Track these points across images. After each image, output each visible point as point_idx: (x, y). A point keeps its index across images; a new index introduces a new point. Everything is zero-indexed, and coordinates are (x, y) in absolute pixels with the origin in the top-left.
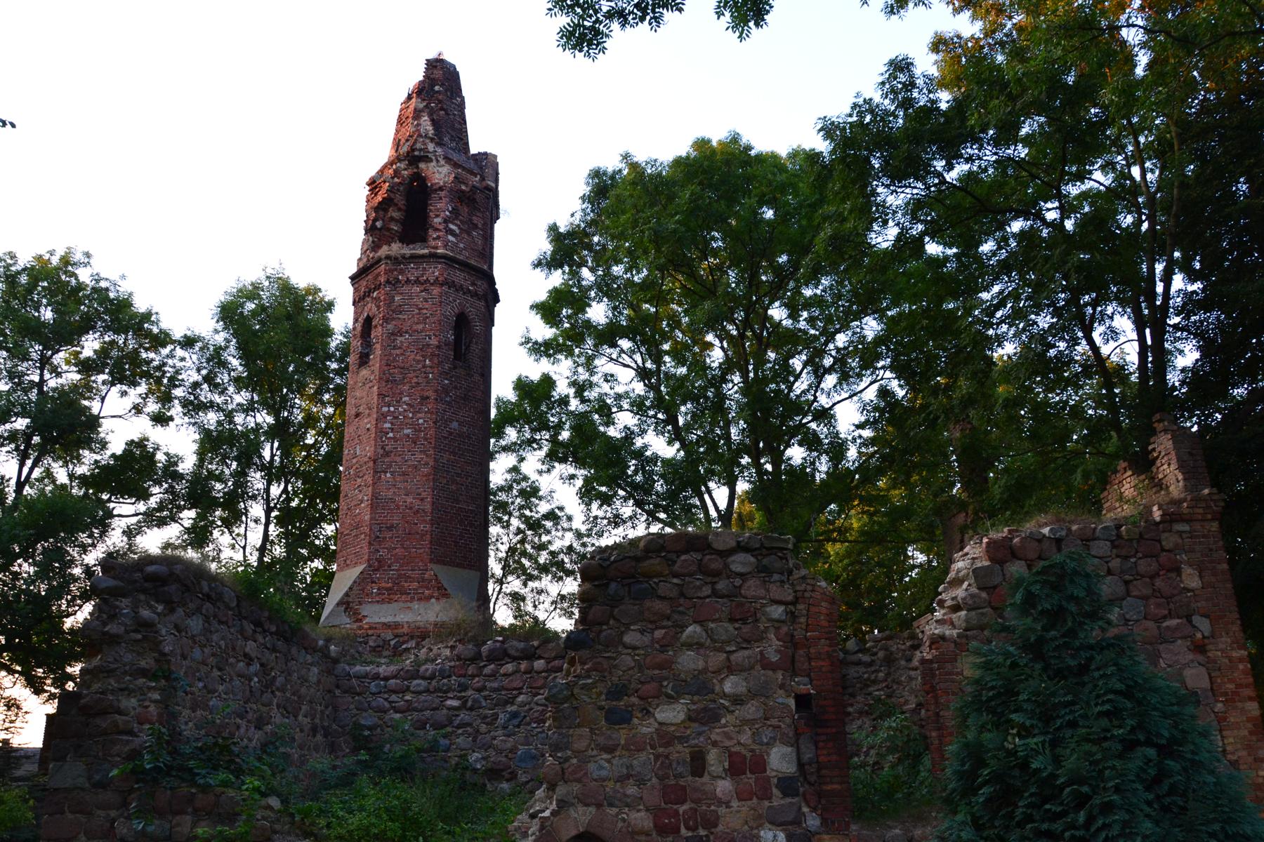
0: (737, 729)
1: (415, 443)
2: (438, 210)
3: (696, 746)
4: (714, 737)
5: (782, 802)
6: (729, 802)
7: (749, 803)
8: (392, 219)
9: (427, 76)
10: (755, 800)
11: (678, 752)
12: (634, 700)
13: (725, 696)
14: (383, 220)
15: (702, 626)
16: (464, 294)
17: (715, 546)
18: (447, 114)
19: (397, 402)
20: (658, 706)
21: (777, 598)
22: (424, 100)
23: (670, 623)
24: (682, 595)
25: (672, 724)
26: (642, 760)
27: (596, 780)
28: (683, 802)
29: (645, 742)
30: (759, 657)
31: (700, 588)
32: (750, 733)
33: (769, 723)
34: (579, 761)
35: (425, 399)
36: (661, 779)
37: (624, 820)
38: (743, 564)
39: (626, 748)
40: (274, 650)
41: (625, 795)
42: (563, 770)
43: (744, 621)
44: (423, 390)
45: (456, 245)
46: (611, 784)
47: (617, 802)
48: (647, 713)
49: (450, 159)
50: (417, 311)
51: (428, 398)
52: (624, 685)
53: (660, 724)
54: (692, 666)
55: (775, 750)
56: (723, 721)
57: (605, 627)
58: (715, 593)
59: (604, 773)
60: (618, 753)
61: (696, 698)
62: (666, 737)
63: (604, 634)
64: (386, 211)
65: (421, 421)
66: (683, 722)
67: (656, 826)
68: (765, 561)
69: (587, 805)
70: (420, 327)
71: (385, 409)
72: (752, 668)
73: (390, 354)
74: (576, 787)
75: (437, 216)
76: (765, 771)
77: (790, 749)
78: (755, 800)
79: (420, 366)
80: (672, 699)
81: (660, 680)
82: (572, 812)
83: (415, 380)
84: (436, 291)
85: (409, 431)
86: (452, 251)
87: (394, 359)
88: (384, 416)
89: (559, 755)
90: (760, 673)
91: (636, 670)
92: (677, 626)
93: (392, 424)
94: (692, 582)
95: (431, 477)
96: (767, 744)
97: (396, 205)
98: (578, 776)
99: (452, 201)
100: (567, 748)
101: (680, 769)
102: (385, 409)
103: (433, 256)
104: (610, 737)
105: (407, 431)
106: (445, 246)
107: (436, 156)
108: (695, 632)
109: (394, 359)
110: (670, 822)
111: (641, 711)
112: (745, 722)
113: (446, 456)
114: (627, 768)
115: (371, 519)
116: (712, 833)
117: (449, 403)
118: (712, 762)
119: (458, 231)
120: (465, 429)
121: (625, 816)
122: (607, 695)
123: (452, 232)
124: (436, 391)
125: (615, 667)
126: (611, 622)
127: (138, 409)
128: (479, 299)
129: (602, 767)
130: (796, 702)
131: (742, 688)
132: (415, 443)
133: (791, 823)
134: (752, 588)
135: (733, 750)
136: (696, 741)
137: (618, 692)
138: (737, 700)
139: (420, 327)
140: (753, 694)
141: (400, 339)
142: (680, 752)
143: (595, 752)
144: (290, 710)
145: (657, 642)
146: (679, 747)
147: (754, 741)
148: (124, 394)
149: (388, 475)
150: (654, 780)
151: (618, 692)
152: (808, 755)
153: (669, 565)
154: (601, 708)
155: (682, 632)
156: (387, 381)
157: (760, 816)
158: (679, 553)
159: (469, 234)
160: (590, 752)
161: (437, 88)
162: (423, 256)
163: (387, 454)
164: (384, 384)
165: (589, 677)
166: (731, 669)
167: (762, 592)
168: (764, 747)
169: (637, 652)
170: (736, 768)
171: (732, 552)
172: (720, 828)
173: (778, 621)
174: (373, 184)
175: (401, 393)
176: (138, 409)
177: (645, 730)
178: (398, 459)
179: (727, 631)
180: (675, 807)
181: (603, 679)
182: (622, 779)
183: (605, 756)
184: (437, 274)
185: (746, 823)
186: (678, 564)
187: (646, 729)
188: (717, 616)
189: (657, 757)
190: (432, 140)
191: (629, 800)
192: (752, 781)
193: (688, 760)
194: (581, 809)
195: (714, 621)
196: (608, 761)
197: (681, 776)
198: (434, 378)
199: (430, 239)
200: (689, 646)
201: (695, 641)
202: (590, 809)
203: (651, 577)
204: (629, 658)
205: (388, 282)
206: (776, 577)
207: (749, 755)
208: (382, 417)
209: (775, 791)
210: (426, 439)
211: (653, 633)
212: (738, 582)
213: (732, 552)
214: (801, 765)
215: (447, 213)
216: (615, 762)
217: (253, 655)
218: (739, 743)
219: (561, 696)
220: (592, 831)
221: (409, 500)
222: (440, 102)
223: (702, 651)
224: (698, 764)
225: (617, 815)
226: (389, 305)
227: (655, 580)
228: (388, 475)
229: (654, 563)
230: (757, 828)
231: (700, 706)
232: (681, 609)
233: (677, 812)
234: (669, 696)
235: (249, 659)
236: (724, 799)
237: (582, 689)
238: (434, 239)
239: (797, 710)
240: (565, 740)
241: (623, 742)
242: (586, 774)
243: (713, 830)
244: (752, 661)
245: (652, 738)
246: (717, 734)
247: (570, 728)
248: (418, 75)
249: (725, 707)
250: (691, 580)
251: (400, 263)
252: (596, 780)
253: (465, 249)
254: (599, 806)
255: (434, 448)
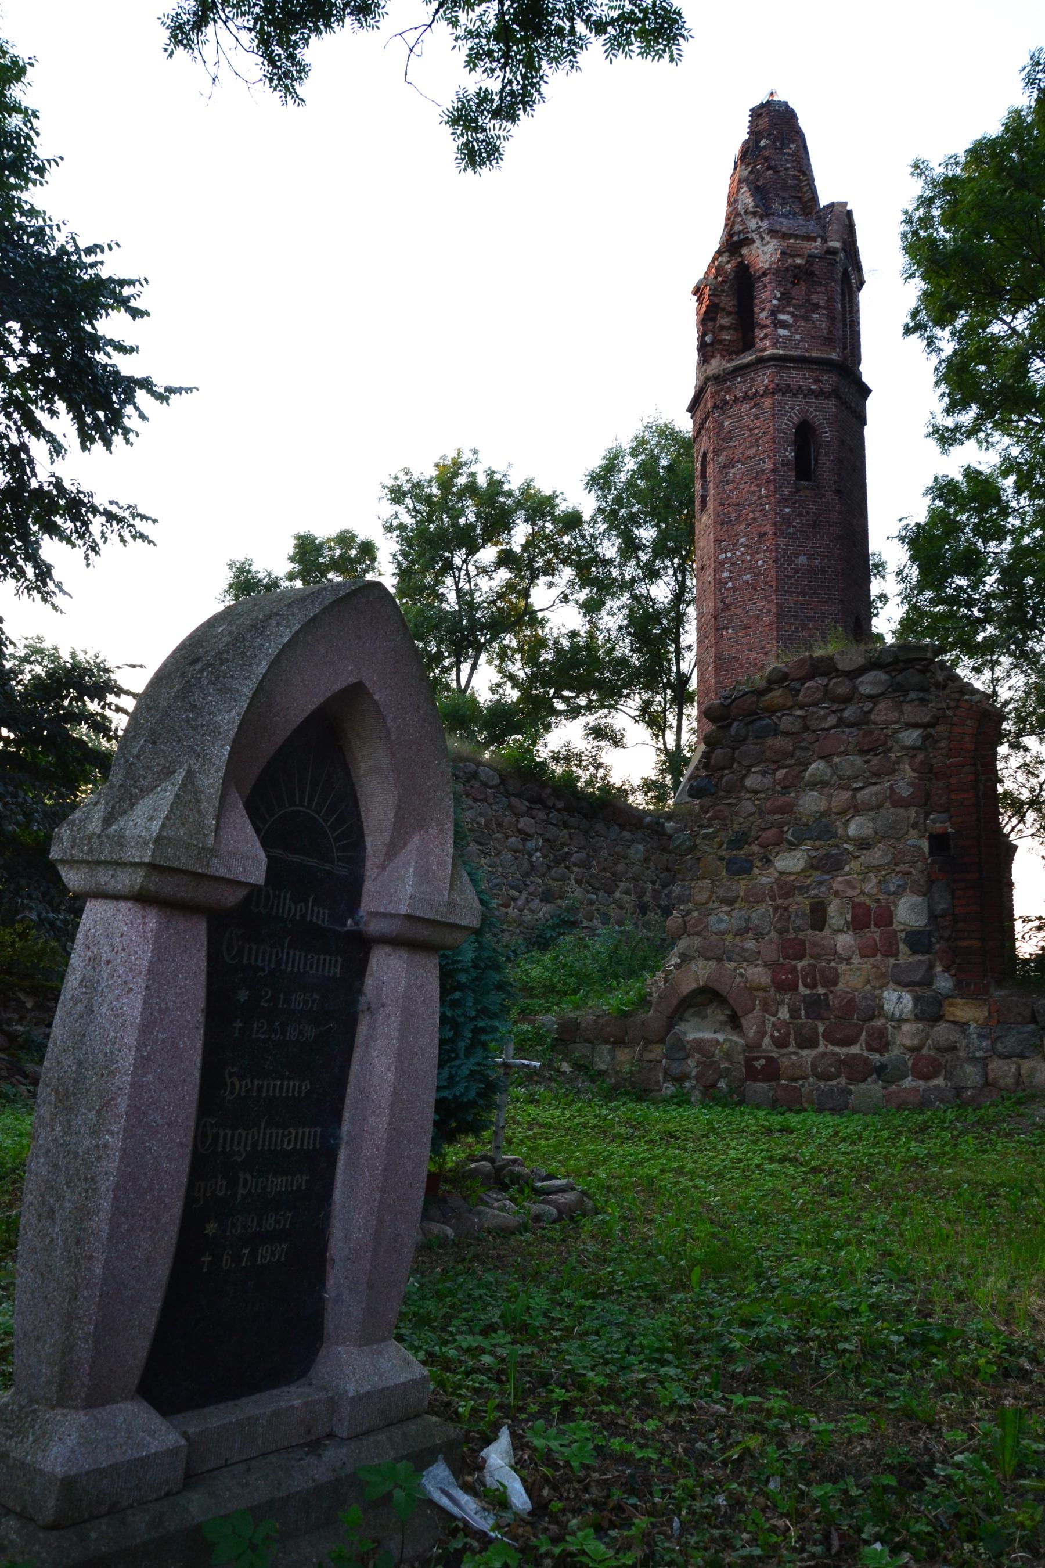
0: (860, 877)
1: (755, 589)
2: (763, 302)
3: (816, 896)
4: (836, 886)
5: (910, 960)
6: (850, 958)
7: (872, 959)
8: (722, 328)
9: (755, 133)
10: (879, 957)
11: (797, 904)
12: (755, 848)
13: (849, 840)
14: (713, 332)
15: (827, 761)
16: (805, 396)
17: (840, 666)
18: (776, 172)
19: (735, 545)
20: (777, 854)
21: (912, 720)
22: (749, 164)
23: (793, 761)
24: (806, 728)
25: (791, 874)
26: (761, 913)
27: (715, 933)
28: (801, 958)
29: (764, 893)
30: (888, 792)
31: (825, 718)
32: (875, 881)
33: (898, 869)
34: (700, 914)
35: (762, 535)
36: (780, 932)
37: (742, 975)
38: (874, 684)
39: (745, 900)
40: (566, 825)
41: (743, 950)
42: (685, 923)
43: (872, 750)
44: (760, 526)
45: (789, 338)
46: (729, 938)
47: (735, 957)
48: (768, 862)
49: (777, 232)
50: (748, 433)
51: (765, 534)
52: (744, 833)
53: (781, 873)
54: (815, 808)
55: (903, 900)
56: (847, 868)
57: (726, 772)
58: (841, 723)
59: (723, 926)
60: (737, 905)
61: (818, 843)
62: (786, 888)
63: (725, 779)
64: (714, 319)
65: (760, 563)
66: (803, 871)
67: (773, 981)
68: (900, 678)
69: (708, 959)
70: (753, 451)
71: (722, 556)
72: (880, 806)
73: (724, 491)
74: (697, 941)
75: (763, 309)
76: (891, 923)
77: (920, 899)
78: (879, 957)
79: (756, 498)
80: (793, 846)
81: (780, 825)
82: (693, 967)
83: (751, 516)
84: (767, 402)
85: (749, 576)
86: (785, 348)
87: (728, 496)
88: (722, 564)
89: (682, 908)
90: (889, 812)
91: (757, 816)
92: (800, 764)
93: (730, 572)
94: (816, 713)
95: (774, 626)
96: (894, 893)
97: (724, 309)
98: (699, 929)
99: (780, 284)
100: (689, 901)
101: (799, 922)
102: (722, 556)
103: (760, 360)
104: (729, 888)
105: (746, 577)
106: (775, 345)
107: (760, 233)
108: (818, 769)
109: (728, 496)
110: (787, 978)
111: (761, 860)
112: (871, 869)
113: (793, 598)
114: (746, 920)
115: (716, 683)
116: (832, 992)
117: (793, 536)
118: (832, 915)
119: (791, 321)
120: (817, 563)
121: (742, 970)
122: (728, 844)
123: (783, 325)
124: (775, 524)
125: (736, 813)
126: (735, 766)
127: (565, 598)
128: (827, 398)
129: (721, 920)
130: (930, 844)
131: (867, 831)
132: (755, 589)
133: (920, 984)
134: (883, 712)
135: (857, 900)
136: (816, 891)
137: (739, 841)
138: (863, 844)
139: (753, 451)
140: (881, 836)
141: (733, 471)
142: (800, 903)
143: (716, 905)
144: (597, 885)
145: (778, 784)
146: (799, 898)
147: (880, 891)
148: (550, 585)
149: (730, 631)
150: (773, 934)
151: (739, 841)
152: (941, 907)
153: (794, 696)
154: (721, 858)
155: (805, 770)
156: (722, 524)
157: (883, 975)
158: (803, 680)
159: (807, 319)
160: (711, 905)
161: (762, 143)
162: (749, 365)
163: (727, 607)
164: (719, 527)
165: (711, 826)
166: (855, 809)
167: (894, 715)
168: (892, 897)
169: (758, 796)
170: (859, 922)
171: (862, 671)
172: (841, 986)
173: (913, 748)
174: (698, 291)
175: (738, 534)
176: (565, 598)
177: (764, 880)
178: (739, 611)
179: (852, 765)
180: (794, 962)
181: (724, 827)
182: (742, 932)
183: (726, 909)
184: (766, 382)
185: (868, 982)
186: (802, 693)
187: (766, 879)
188: (842, 749)
189: (776, 909)
190: (754, 214)
191: (747, 954)
192: (876, 936)
193: (808, 912)
194: (701, 963)
195: (839, 754)
196: (728, 914)
197: (798, 929)
198: (771, 509)
199: (757, 341)
200: (812, 785)
201: (819, 779)
202: (711, 963)
203: (774, 712)
204: (749, 803)
205: (715, 406)
206: (912, 695)
207: (874, 906)
208: (720, 566)
209: (902, 947)
210: (766, 583)
211: (774, 774)
212: (868, 705)
213: (862, 671)
214: (933, 917)
215: (775, 302)
216: (734, 914)
217: (531, 831)
218: (862, 893)
219: (684, 848)
220: (711, 985)
221: (753, 655)
222: (767, 159)
223: (825, 791)
224: (818, 916)
225: (735, 969)
226: (717, 434)
227: (778, 714)
228: (730, 631)
229: (776, 695)
230: (881, 988)
231: (822, 852)
232: (803, 744)
233: (795, 968)
234: (791, 843)
235: (526, 836)
236: (845, 955)
237: (704, 838)
238: (762, 339)
239: (932, 852)
240: (687, 892)
241: (742, 894)
242: (706, 927)
243: (832, 988)
244: (880, 797)
245: (772, 890)
246: (840, 883)
247: (692, 880)
248: (741, 133)
249: (849, 853)
250: (815, 709)
251: (726, 381)
252: (715, 933)
253: (803, 339)
254: (719, 960)
255: (776, 591)
